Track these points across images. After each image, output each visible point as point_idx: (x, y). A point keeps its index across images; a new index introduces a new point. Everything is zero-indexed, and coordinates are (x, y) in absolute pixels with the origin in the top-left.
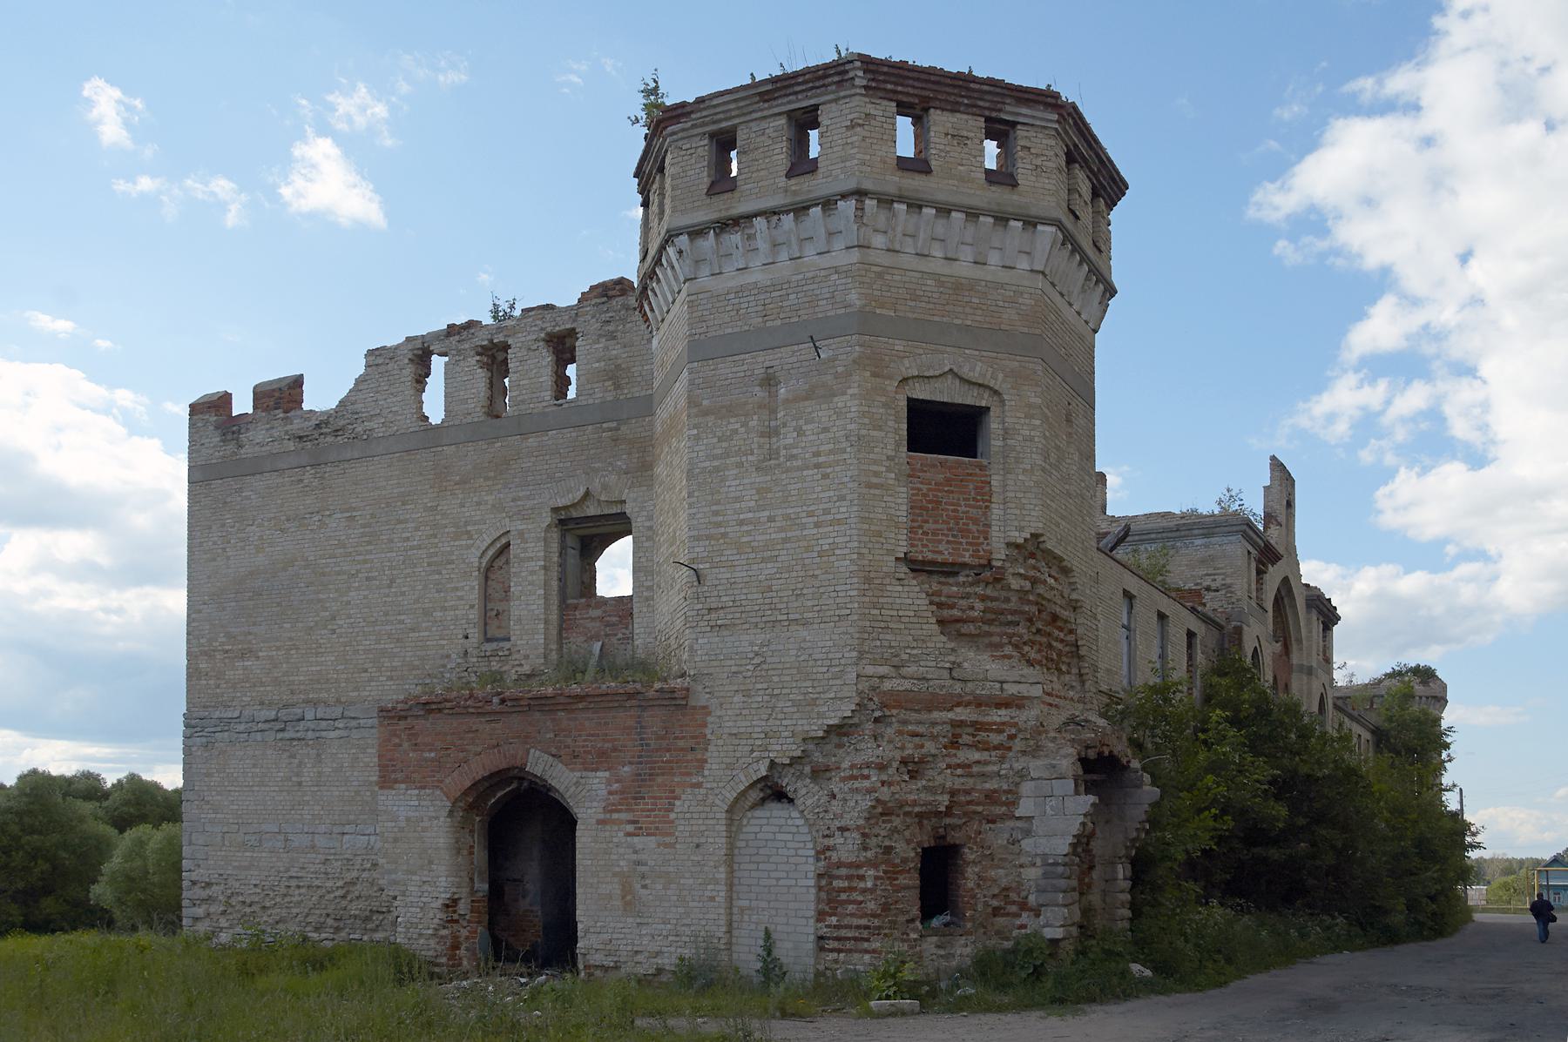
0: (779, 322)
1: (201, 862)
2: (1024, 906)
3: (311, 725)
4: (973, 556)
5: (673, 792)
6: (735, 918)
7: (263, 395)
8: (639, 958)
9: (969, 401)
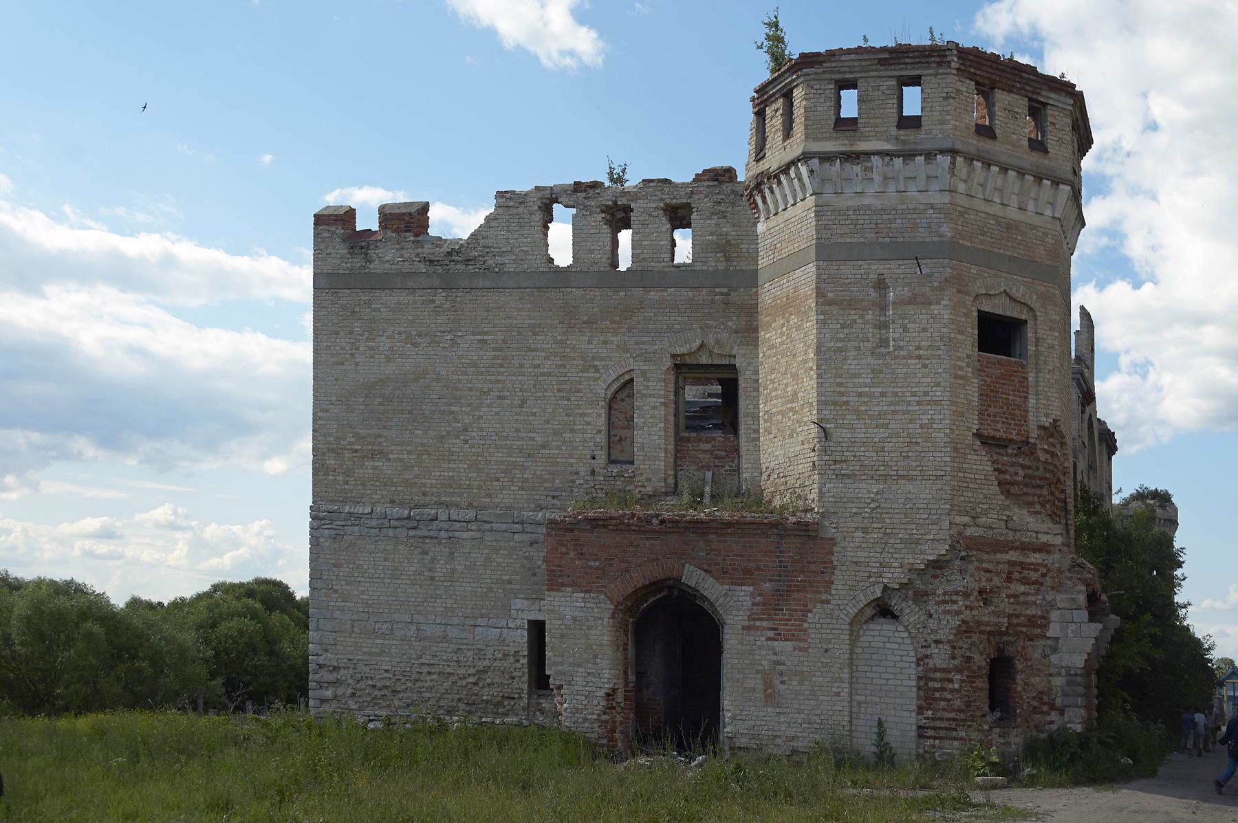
0: (888, 240)
1: (329, 647)
2: (1052, 707)
3: (445, 526)
4: (1017, 434)
5: (806, 606)
6: (854, 710)
7: (389, 216)
8: (779, 741)
9: (1015, 315)
